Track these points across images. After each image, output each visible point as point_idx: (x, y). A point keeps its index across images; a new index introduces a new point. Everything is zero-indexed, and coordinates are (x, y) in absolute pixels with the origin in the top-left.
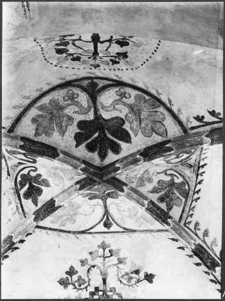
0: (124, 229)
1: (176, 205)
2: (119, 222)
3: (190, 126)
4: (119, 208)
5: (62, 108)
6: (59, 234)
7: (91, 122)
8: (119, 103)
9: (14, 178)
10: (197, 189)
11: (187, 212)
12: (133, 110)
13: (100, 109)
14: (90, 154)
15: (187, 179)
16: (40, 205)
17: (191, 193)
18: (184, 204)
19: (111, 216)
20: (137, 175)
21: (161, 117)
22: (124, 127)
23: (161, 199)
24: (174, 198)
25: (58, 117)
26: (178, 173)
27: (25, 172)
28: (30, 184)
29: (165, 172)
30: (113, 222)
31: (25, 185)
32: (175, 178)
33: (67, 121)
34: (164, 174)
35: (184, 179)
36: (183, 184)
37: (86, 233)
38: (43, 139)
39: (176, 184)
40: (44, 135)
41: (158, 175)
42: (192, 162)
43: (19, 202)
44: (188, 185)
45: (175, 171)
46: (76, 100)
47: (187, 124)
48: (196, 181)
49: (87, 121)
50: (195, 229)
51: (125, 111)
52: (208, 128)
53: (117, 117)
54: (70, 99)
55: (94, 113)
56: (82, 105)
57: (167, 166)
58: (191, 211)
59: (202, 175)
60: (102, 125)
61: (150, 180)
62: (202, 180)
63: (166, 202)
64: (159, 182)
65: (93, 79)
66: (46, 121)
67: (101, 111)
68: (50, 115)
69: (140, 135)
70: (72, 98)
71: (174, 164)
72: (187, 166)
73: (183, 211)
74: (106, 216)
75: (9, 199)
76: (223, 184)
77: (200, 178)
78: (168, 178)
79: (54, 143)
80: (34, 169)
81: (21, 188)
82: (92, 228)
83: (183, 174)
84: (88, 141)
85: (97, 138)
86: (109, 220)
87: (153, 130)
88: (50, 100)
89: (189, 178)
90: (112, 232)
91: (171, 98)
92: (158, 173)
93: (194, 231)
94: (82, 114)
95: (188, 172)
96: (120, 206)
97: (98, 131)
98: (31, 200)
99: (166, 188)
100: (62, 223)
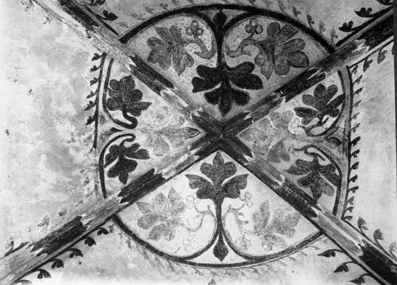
0: (246, 257)
1: (325, 192)
2: (238, 245)
3: (336, 41)
4: (240, 217)
5: (183, 43)
6: (145, 253)
7: (214, 70)
8: (249, 42)
9: (101, 151)
10: (352, 176)
11: (343, 203)
12: (264, 49)
13: (225, 54)
14: (209, 105)
15: (337, 162)
16: (129, 181)
17: (345, 179)
18: (337, 194)
19: (225, 236)
20: (268, 146)
21: (300, 45)
22: (254, 73)
23: (304, 183)
24: (321, 184)
25: (176, 51)
26: (322, 152)
27: (118, 143)
28: (122, 158)
29: (305, 149)
30: (229, 248)
31: (113, 160)
32: (319, 159)
33: (186, 60)
34: (303, 152)
35: (332, 161)
36: (331, 167)
37: (186, 263)
38: (156, 66)
39: (322, 167)
40: (157, 63)
41: (296, 153)
42: (339, 134)
43: (99, 181)
44: (339, 169)
45: (319, 149)
46: (200, 37)
47: (332, 41)
48: (349, 164)
49: (208, 68)
50: (359, 227)
51: (255, 51)
52: (359, 34)
53: (245, 63)
54: (193, 33)
55: (218, 60)
56: (205, 47)
57: (308, 141)
58: (349, 203)
59: (356, 156)
60: (226, 76)
61: (286, 158)
62: (357, 164)
63: (311, 187)
64: (298, 162)
65: (222, 9)
66: (163, 50)
67: (226, 57)
68: (168, 45)
69: (274, 76)
70: (196, 32)
71: (316, 138)
72: (334, 142)
73: (337, 202)
74: (218, 237)
75: (87, 178)
76: (395, 68)
77: (353, 160)
78: (310, 159)
79: (168, 77)
80: (130, 137)
81: (108, 164)
82: (196, 255)
83: (329, 154)
84: (210, 91)
85: (219, 89)
86: (223, 243)
87: (290, 64)
88: (172, 26)
89: (338, 160)
90: (226, 266)
91: (311, 14)
92: (296, 150)
93: (359, 229)
94: (204, 58)
95: (335, 151)
96: (240, 214)
97: (221, 82)
98: (118, 177)
99: (308, 171)
100: (152, 232)
